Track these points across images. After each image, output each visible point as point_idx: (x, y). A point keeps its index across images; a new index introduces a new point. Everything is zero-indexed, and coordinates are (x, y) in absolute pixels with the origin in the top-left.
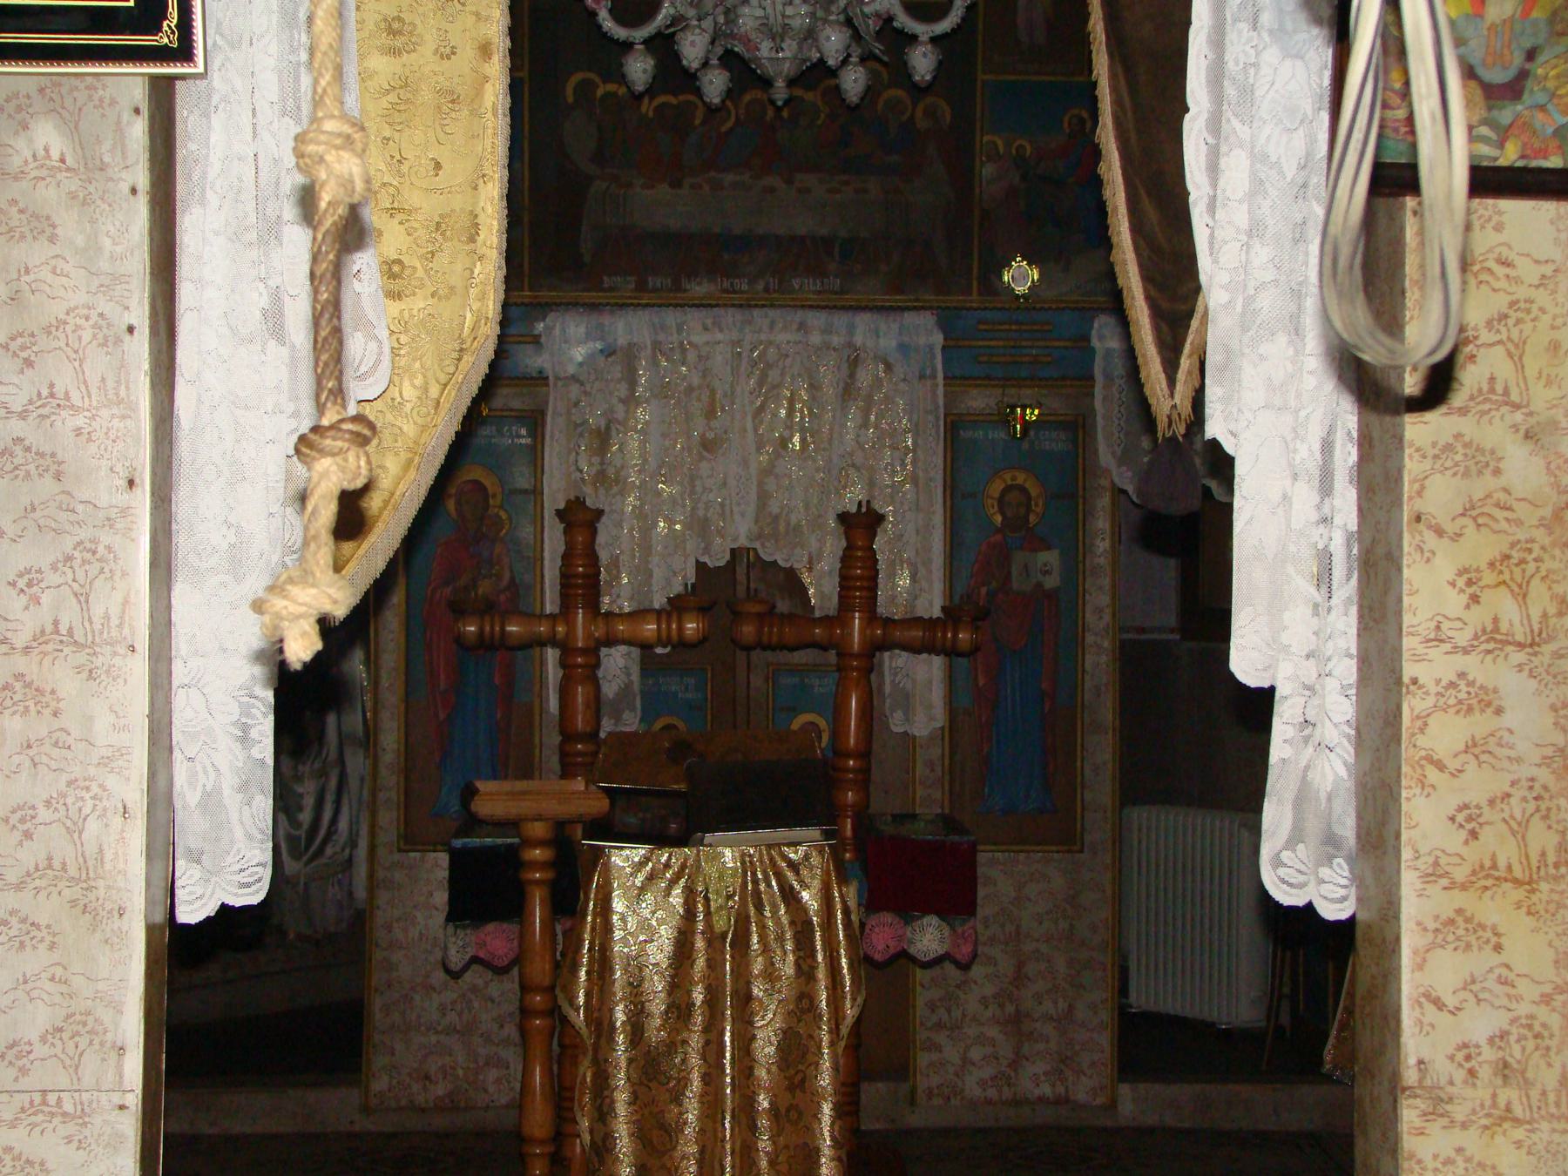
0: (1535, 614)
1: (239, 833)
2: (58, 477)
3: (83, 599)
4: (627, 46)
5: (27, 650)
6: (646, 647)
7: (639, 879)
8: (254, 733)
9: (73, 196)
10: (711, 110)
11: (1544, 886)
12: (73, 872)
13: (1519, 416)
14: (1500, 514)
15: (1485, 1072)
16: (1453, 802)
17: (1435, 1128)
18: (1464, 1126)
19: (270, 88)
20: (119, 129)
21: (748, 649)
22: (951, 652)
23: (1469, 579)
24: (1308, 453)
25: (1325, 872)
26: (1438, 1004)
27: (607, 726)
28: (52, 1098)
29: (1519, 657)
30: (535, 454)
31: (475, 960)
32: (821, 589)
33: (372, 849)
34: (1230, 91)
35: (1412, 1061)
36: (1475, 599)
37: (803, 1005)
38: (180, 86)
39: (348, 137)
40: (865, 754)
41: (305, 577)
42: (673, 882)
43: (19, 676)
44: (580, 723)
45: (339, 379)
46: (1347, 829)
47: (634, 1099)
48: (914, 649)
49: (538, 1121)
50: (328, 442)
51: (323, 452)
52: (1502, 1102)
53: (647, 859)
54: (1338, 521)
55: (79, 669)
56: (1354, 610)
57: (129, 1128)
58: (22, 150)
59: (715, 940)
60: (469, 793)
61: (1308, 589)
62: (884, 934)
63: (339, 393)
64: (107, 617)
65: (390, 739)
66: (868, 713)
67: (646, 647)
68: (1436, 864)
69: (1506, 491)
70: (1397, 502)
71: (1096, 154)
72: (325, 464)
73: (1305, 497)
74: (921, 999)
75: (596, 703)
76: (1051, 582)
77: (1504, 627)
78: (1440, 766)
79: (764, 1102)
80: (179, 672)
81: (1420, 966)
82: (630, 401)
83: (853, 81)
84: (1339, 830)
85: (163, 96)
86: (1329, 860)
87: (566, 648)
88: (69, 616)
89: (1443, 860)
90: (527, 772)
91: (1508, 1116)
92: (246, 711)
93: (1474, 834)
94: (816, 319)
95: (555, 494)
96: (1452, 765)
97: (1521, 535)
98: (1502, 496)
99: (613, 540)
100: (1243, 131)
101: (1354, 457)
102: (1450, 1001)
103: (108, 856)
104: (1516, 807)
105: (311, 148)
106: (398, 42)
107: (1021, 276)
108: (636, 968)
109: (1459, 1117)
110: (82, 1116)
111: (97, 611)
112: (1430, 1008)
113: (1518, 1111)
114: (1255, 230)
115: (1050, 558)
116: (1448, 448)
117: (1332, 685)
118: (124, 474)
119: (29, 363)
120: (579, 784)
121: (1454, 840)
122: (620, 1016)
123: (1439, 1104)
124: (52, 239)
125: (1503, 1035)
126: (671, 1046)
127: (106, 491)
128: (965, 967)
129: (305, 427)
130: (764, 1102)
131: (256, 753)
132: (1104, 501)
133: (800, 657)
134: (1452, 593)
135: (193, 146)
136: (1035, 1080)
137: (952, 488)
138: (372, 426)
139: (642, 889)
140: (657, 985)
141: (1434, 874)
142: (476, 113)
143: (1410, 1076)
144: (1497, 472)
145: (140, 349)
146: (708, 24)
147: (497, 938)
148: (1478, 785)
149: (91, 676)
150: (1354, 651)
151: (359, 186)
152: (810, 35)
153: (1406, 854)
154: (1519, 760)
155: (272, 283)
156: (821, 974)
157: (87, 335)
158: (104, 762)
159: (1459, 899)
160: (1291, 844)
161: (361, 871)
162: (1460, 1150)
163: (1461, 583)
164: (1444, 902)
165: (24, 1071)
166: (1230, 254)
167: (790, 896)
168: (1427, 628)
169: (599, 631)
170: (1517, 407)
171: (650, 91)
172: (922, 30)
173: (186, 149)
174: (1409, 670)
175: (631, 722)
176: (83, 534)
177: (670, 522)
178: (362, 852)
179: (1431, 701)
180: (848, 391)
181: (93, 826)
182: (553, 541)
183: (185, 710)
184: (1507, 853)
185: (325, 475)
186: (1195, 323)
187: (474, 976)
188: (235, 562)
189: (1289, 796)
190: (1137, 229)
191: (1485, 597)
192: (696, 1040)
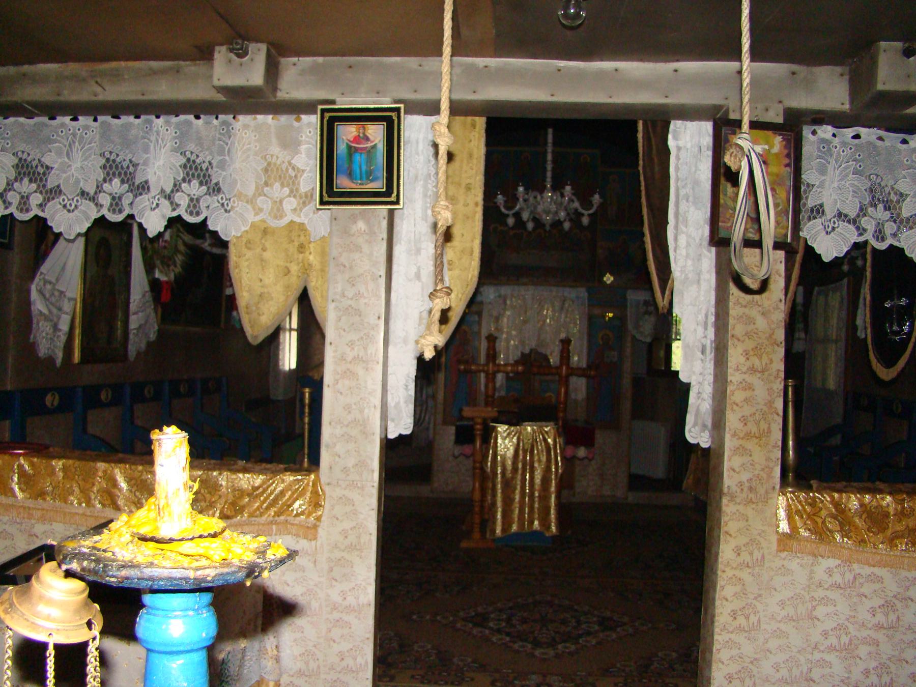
0: (764, 364)
1: (405, 415)
2: (360, 316)
3: (365, 349)
4: (508, 216)
5: (351, 362)
6: (507, 373)
7: (505, 435)
8: (409, 387)
9: (367, 241)
10: (530, 232)
11: (764, 439)
12: (361, 423)
13: (760, 308)
14: (755, 335)
15: (745, 490)
16: (740, 415)
17: (731, 504)
18: (739, 504)
19: (419, 212)
20: (379, 223)
21: (534, 374)
22: (587, 377)
23: (746, 353)
24: (701, 318)
25: (702, 434)
26: (734, 470)
27: (497, 394)
28: (355, 483)
29: (759, 375)
30: (479, 323)
31: (461, 454)
32: (554, 360)
33: (435, 425)
34: (681, 218)
35: (726, 486)
36: (748, 359)
37: (548, 470)
38: (396, 212)
39: (447, 206)
40: (565, 403)
41: (431, 334)
42: (514, 436)
43: (348, 369)
44: (490, 393)
45: (442, 276)
46: (709, 423)
47: (503, 492)
48: (579, 376)
49: (477, 496)
50: (439, 294)
51: (437, 297)
52: (749, 498)
53: (507, 429)
54: (708, 337)
55: (364, 368)
56: (713, 362)
57: (375, 492)
58: (354, 229)
59: (525, 451)
60: (461, 410)
61: (699, 354)
62: (570, 451)
63: (442, 280)
64: (371, 354)
65: (440, 396)
66: (566, 393)
67: (507, 373)
68: (735, 432)
69: (756, 329)
70: (727, 331)
71: (643, 235)
72: (437, 301)
73: (700, 330)
74: (577, 470)
75: (494, 389)
76: (615, 359)
77: (755, 366)
78: (737, 405)
79: (537, 494)
80: (390, 370)
81: (730, 460)
82: (505, 310)
83: (567, 225)
84: (706, 423)
85: (391, 213)
86: (703, 431)
87: (487, 373)
88: (362, 354)
89: (737, 431)
90: (475, 405)
91: (751, 501)
92: (407, 381)
93: (746, 424)
94: (554, 289)
95: (484, 332)
96: (740, 405)
97: (761, 341)
98: (756, 331)
99: (501, 345)
100: (684, 229)
101: (714, 319)
102: (737, 470)
103: (371, 418)
104: (757, 417)
105: (437, 209)
106: (454, 202)
107: (609, 279)
108: (504, 458)
109: (738, 501)
110: (362, 488)
111: (369, 352)
112: (732, 472)
113: (754, 500)
114: (687, 256)
115: (615, 353)
116: (741, 317)
117: (706, 383)
118: (377, 315)
119: (353, 285)
120: (490, 409)
121: (740, 426)
122: (499, 471)
123: (733, 498)
124: (361, 252)
125: (751, 479)
126: (513, 478)
127: (372, 320)
128: (590, 460)
129: (432, 291)
130: (537, 494)
131: (410, 393)
132: (629, 339)
133: (549, 377)
134: (742, 357)
135: (398, 228)
136: (607, 491)
137: (590, 335)
138: (451, 291)
139: (506, 437)
140: (509, 463)
141: (734, 435)
142: (474, 221)
143: (725, 490)
144: (754, 324)
145: (383, 281)
146: (529, 210)
147: (467, 449)
148: (747, 410)
149: (367, 370)
150: (712, 373)
151: (450, 221)
152: (556, 213)
153: (727, 429)
154: (758, 404)
155: (418, 265)
156: (553, 461)
157: (369, 278)
158: (370, 393)
159: (741, 442)
160: (694, 426)
161: (431, 431)
162: (738, 510)
163: (744, 354)
164: (737, 442)
165: (348, 475)
166: (681, 262)
167: (545, 440)
168: (734, 367)
169: (496, 369)
170: (760, 306)
171: (512, 228)
172: (586, 213)
173: (396, 229)
174: (729, 378)
175: (503, 393)
176: (366, 331)
177: (514, 342)
178: (432, 425)
179: (735, 387)
180: (562, 308)
181: (366, 411)
182: (484, 345)
183: (391, 380)
184: (754, 429)
185: (437, 304)
186: (670, 282)
187: (461, 459)
188: (405, 341)
189: (693, 413)
190: (654, 255)
191: (751, 358)
192: (519, 477)
